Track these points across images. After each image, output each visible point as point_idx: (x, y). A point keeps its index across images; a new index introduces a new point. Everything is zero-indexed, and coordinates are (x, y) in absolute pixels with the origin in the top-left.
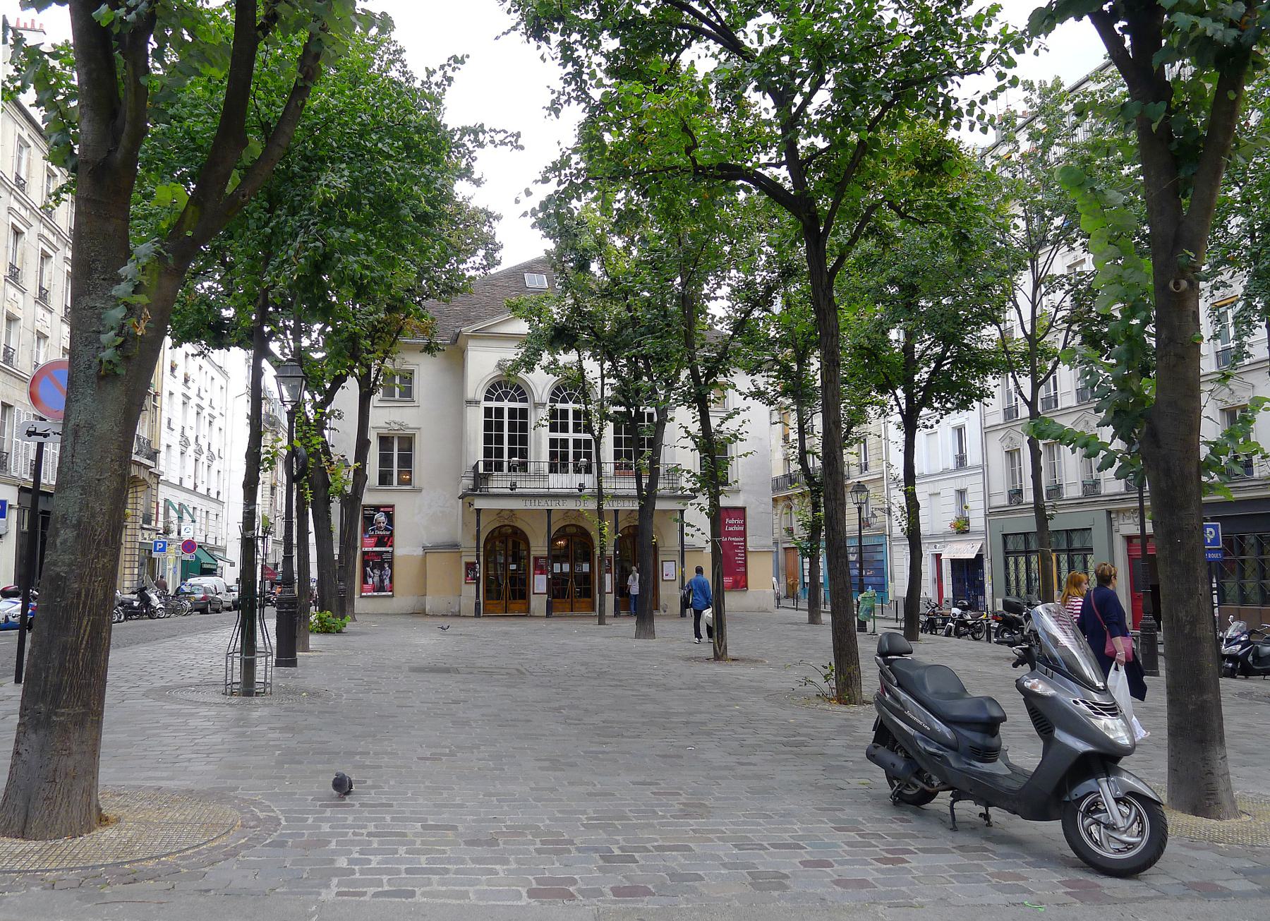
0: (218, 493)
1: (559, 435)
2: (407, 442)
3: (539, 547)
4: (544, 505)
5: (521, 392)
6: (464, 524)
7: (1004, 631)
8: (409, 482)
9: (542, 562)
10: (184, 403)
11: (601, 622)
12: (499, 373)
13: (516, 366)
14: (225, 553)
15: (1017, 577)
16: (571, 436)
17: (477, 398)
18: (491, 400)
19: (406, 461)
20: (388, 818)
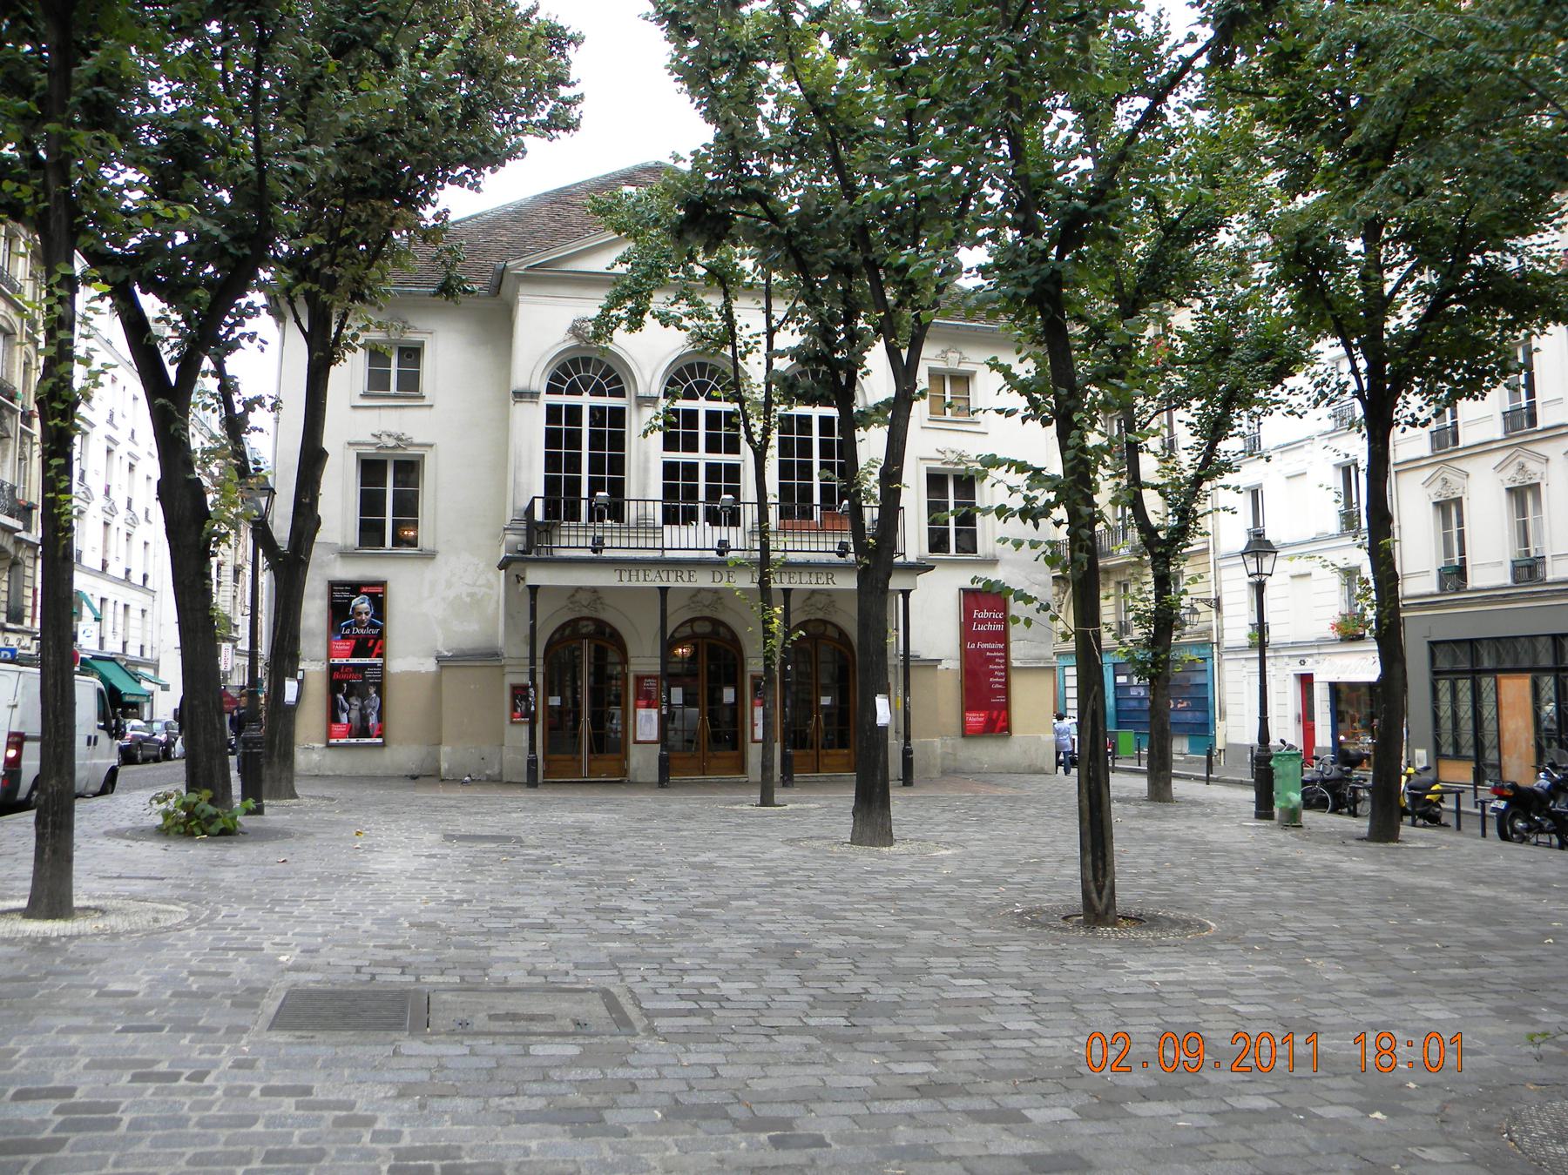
0: (145, 577)
1: (681, 456)
2: (409, 469)
3: (644, 658)
4: (654, 580)
5: (613, 378)
6: (509, 615)
7: (1514, 816)
8: (413, 543)
9: (650, 684)
10: (109, 451)
11: (766, 800)
12: (574, 342)
13: (604, 326)
14: (157, 671)
15: (1455, 714)
16: (702, 457)
17: (534, 388)
18: (559, 392)
19: (408, 506)
20: (367, 1137)
